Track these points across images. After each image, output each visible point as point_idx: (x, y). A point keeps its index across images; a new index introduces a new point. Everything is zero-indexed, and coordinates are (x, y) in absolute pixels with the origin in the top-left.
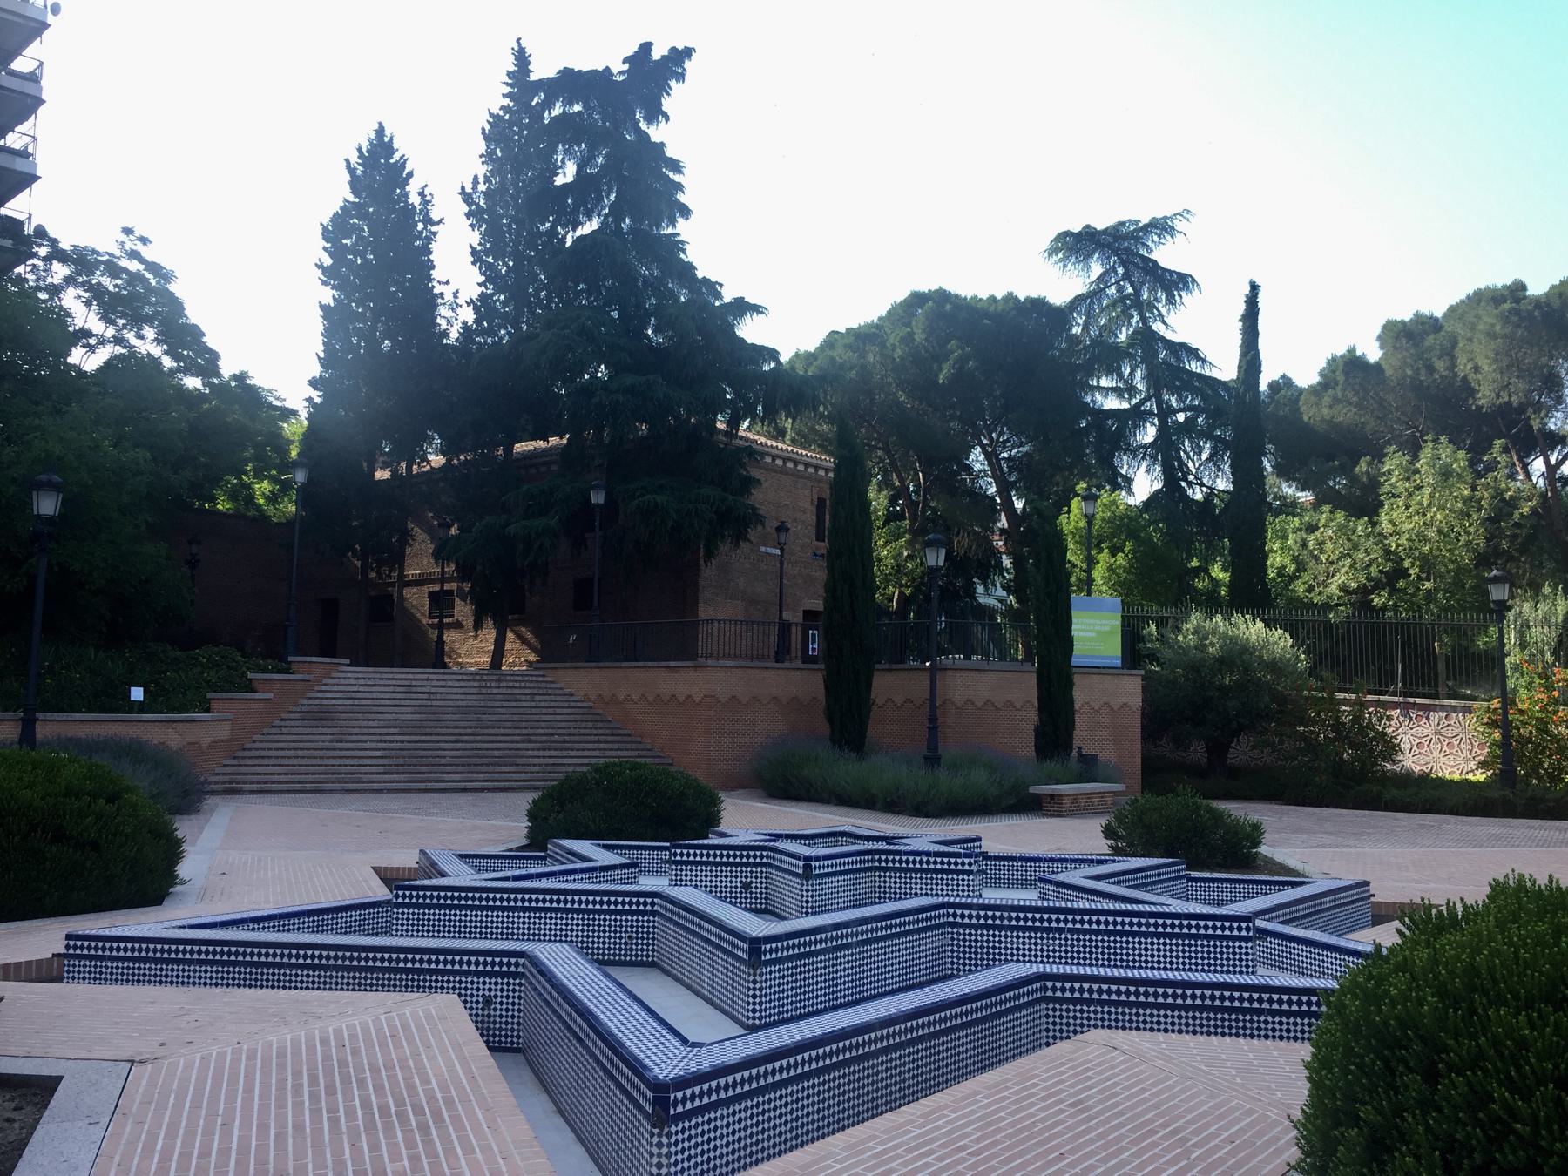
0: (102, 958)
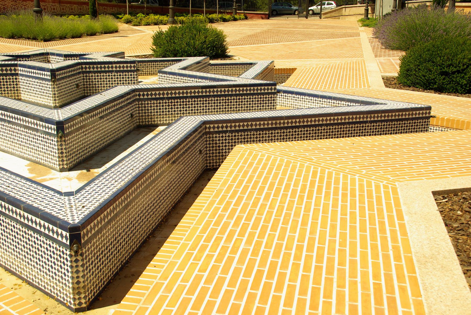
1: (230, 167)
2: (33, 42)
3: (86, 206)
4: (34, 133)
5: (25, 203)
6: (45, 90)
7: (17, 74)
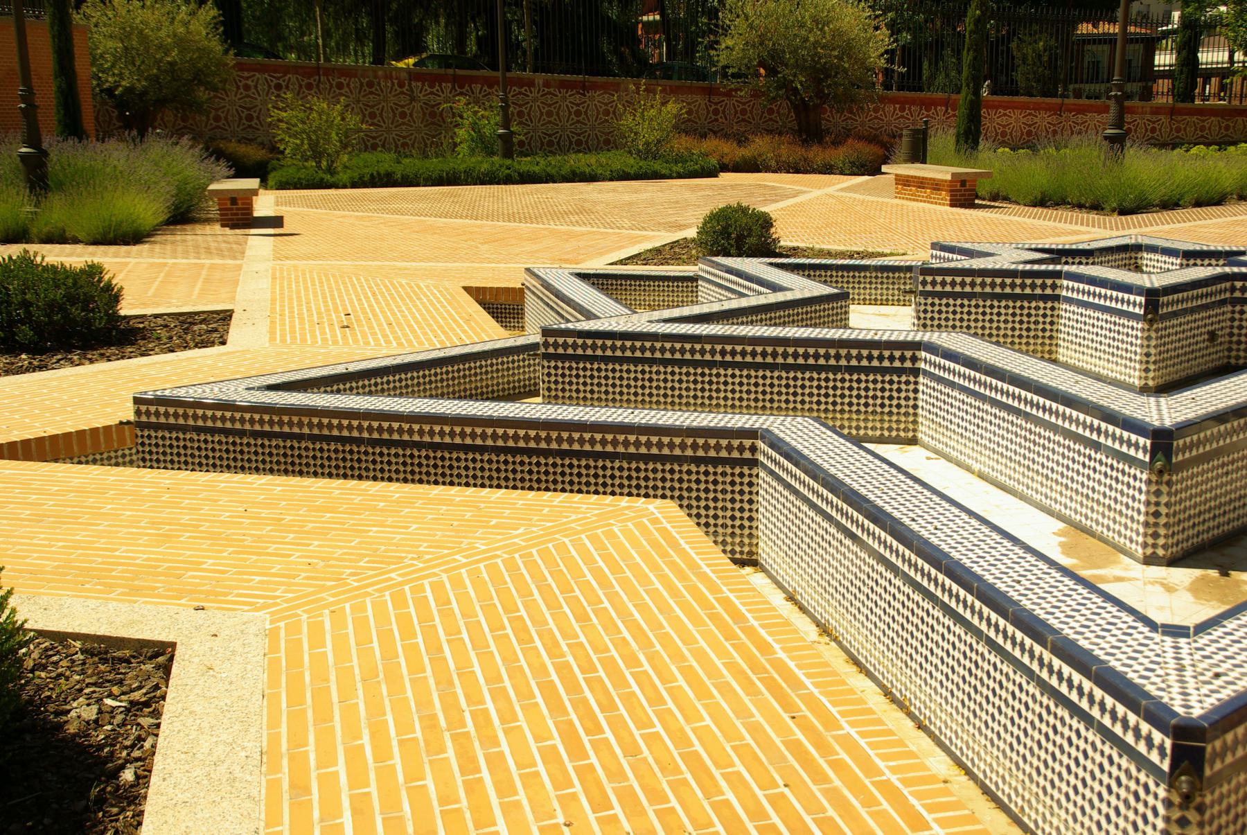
0: (184, 429)
2: (1091, 216)
3: (1226, 675)
4: (1087, 452)
5: (1056, 632)
6: (1123, 342)
7: (1057, 298)
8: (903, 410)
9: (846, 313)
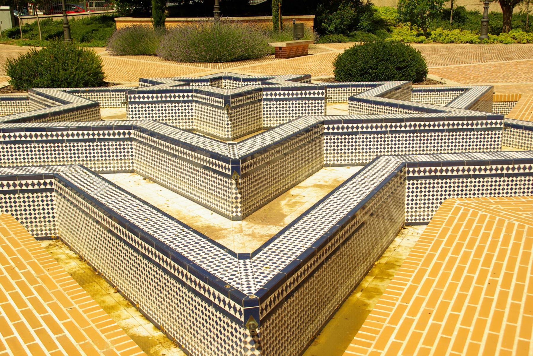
1: (442, 224)
8: (96, 158)
9: (99, 112)
